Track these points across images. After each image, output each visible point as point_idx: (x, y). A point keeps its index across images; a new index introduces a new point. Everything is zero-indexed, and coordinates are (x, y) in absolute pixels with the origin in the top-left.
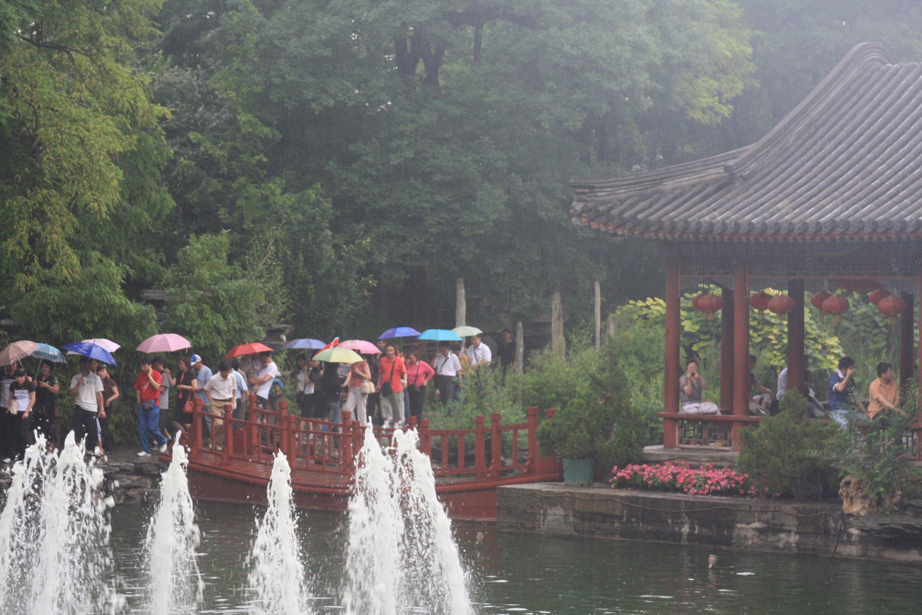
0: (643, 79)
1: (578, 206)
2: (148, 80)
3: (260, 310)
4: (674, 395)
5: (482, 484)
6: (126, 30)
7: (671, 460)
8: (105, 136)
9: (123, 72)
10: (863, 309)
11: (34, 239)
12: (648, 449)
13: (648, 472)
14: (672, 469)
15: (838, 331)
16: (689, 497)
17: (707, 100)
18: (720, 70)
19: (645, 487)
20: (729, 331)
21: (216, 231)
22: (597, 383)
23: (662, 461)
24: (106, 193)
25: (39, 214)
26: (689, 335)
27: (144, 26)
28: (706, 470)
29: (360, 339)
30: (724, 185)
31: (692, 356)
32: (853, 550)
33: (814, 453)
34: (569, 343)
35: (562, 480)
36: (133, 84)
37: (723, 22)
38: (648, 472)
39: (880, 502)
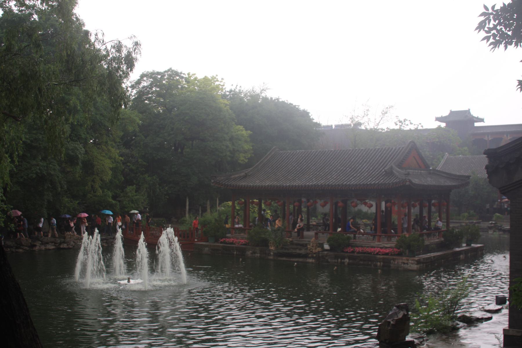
0: (228, 153)
1: (213, 181)
2: (118, 151)
3: (142, 203)
4: (233, 223)
5: (292, 259)
6: (114, 141)
7: (233, 237)
8: (108, 164)
9: (113, 150)
10: (275, 205)
11: (92, 186)
12: (227, 235)
13: (227, 240)
14: (233, 239)
15: (270, 209)
16: (236, 246)
17: (242, 158)
18: (245, 152)
19: (226, 243)
20: (245, 208)
21: (133, 185)
22: (216, 220)
23: (230, 238)
24: (108, 176)
25: (93, 181)
26: (238, 210)
27: (118, 140)
28: (240, 240)
29: (78, 254)
30: (245, 177)
31: (238, 214)
32: (271, 257)
33: (263, 236)
34: (211, 211)
35: (208, 241)
36: (115, 152)
37: (246, 141)
38: (227, 240)
39: (277, 247)
